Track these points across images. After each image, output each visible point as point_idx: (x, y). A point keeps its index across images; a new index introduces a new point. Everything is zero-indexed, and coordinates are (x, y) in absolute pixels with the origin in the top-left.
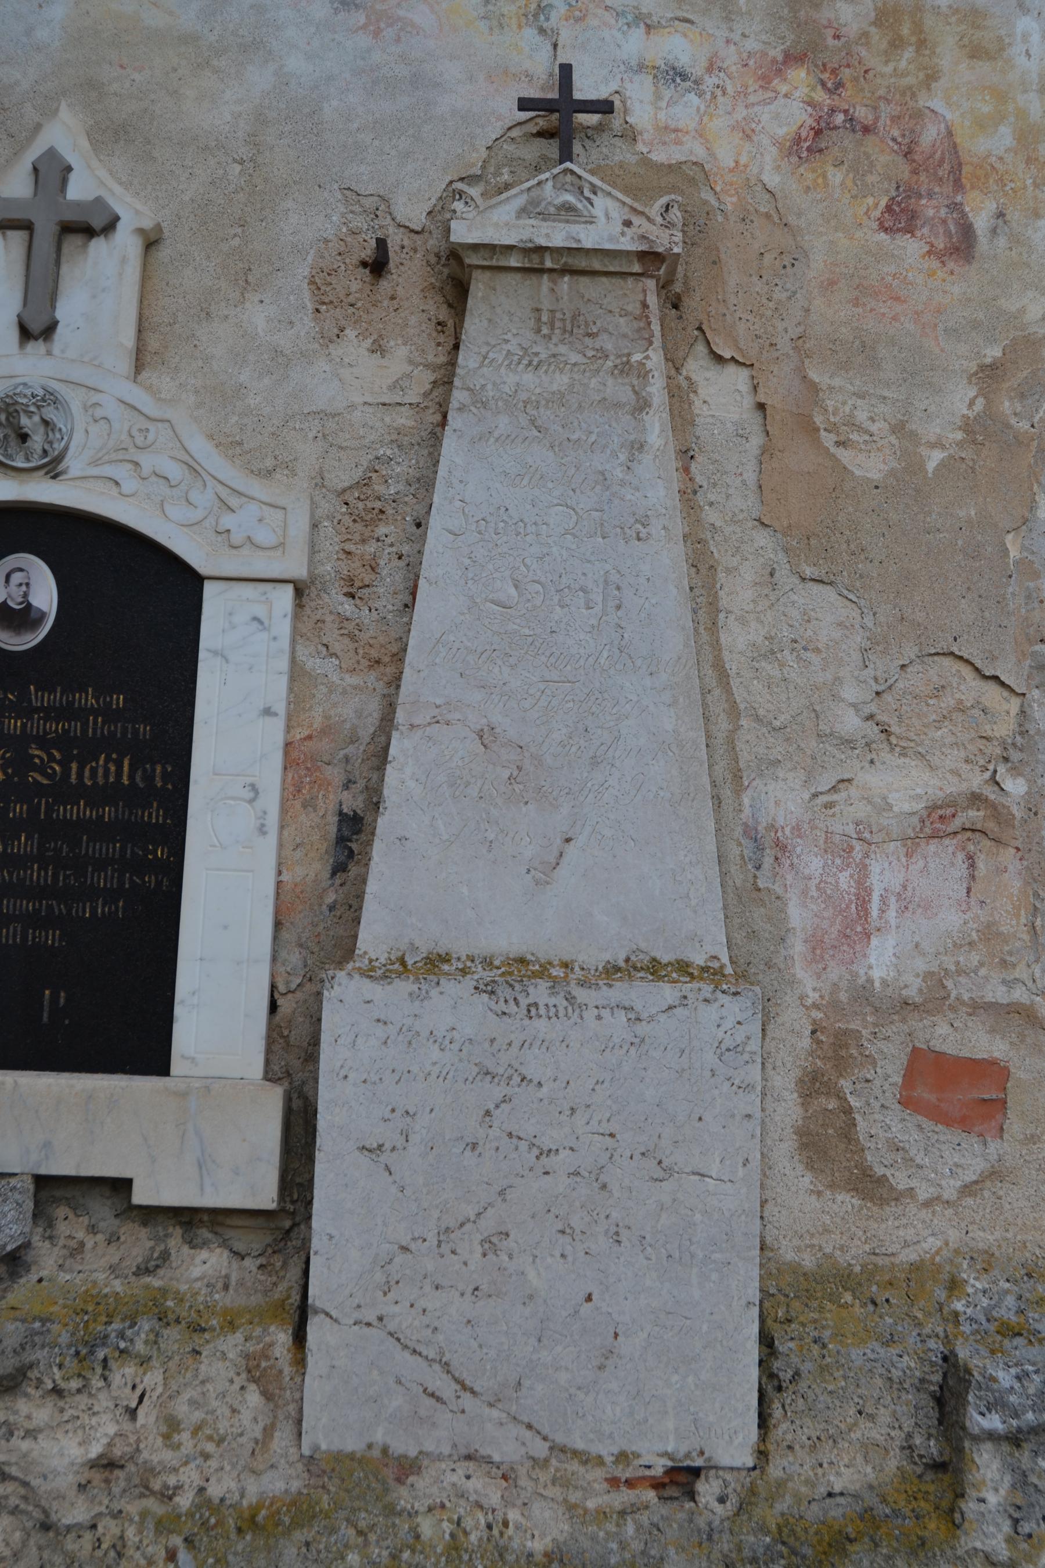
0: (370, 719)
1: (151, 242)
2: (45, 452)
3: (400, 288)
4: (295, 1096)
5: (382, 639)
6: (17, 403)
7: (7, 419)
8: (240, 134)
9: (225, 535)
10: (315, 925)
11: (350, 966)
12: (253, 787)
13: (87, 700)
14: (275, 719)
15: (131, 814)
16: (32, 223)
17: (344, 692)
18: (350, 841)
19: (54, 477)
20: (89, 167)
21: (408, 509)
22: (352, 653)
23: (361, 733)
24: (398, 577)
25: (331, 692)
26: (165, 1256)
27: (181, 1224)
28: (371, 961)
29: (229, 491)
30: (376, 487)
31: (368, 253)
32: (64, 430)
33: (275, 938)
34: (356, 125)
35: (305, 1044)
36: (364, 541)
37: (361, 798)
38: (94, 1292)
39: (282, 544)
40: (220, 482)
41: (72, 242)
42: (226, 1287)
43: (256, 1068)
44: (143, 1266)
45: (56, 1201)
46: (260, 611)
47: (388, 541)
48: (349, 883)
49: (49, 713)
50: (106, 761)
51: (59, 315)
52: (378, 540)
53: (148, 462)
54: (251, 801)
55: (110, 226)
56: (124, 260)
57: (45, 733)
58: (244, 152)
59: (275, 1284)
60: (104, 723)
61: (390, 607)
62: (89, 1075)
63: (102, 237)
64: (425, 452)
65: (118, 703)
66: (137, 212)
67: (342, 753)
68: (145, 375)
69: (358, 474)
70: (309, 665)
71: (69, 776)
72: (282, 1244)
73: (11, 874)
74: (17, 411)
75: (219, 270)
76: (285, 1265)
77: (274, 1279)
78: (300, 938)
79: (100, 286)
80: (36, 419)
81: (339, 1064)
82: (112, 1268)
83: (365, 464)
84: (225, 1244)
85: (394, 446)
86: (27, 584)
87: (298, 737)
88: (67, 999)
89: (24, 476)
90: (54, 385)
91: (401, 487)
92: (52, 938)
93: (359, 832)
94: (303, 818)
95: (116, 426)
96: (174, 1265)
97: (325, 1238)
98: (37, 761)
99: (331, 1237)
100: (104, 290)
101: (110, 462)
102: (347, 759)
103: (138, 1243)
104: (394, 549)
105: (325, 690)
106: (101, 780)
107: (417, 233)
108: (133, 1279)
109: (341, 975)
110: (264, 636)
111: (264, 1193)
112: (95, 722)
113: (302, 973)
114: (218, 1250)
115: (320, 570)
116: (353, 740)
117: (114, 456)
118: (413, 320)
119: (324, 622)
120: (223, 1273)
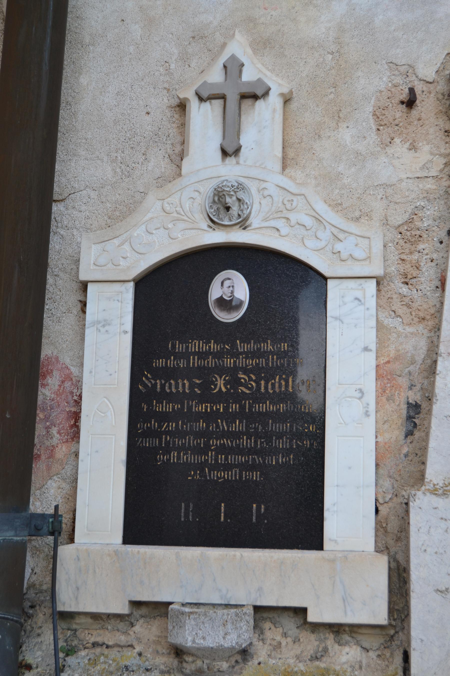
0: (421, 351)
1: (287, 100)
2: (239, 215)
3: (423, 114)
4: (392, 560)
5: (425, 306)
6: (224, 190)
7: (219, 199)
8: (330, 38)
9: (338, 254)
10: (397, 465)
11: (423, 488)
12: (361, 391)
13: (267, 347)
14: (370, 353)
15: (294, 407)
16: (225, 95)
17: (406, 336)
18: (414, 418)
19: (244, 229)
20: (253, 63)
21: (435, 234)
22: (409, 315)
23: (417, 358)
24: (432, 272)
25: (399, 337)
26: (326, 650)
27: (333, 632)
28: (434, 485)
29: (338, 230)
30: (417, 223)
31: (405, 96)
32: (248, 203)
33: (376, 473)
34: (393, 28)
35: (396, 532)
36: (411, 253)
37: (419, 394)
38: (289, 670)
39: (369, 257)
40: (333, 226)
41: (247, 103)
42: (361, 668)
43: (371, 547)
44: (314, 656)
45: (264, 619)
46: (359, 294)
47: (425, 252)
48: (415, 442)
49: (250, 355)
50: (280, 380)
51: (242, 142)
52: (419, 252)
53: (293, 217)
54: (360, 398)
55: (266, 94)
56: (274, 111)
57: (247, 366)
58: (333, 48)
59: (387, 666)
60: (277, 359)
61: (428, 288)
62: (261, 550)
63: (262, 99)
64: (443, 202)
65: (284, 348)
66: (280, 85)
67: (407, 370)
68: (287, 171)
69: (406, 217)
70: (386, 322)
71: (260, 388)
72: (389, 643)
73: (232, 442)
74: (224, 195)
75: (324, 112)
76: (392, 654)
77: (387, 663)
78: (389, 472)
79: (262, 126)
80: (234, 198)
81: (421, 543)
82: (298, 657)
83: (410, 211)
84: (358, 643)
85: (425, 200)
86: (233, 286)
87: (382, 362)
88: (265, 509)
89: (229, 229)
90: (242, 180)
91: (430, 222)
92: (256, 476)
93: (419, 413)
94: (387, 406)
95: (276, 199)
96: (331, 655)
97: (419, 641)
98: (243, 380)
99: (422, 641)
100: (264, 128)
101: (274, 219)
102: (410, 373)
103: (310, 643)
104: (428, 256)
105: (395, 335)
106: (277, 390)
107: (431, 83)
108: (309, 662)
109: (419, 494)
110: (362, 308)
111: (379, 614)
112: (273, 359)
113: (392, 492)
114: (354, 647)
115: (389, 270)
116: (413, 362)
117: (275, 215)
118: (431, 131)
119: (392, 298)
120: (358, 659)
